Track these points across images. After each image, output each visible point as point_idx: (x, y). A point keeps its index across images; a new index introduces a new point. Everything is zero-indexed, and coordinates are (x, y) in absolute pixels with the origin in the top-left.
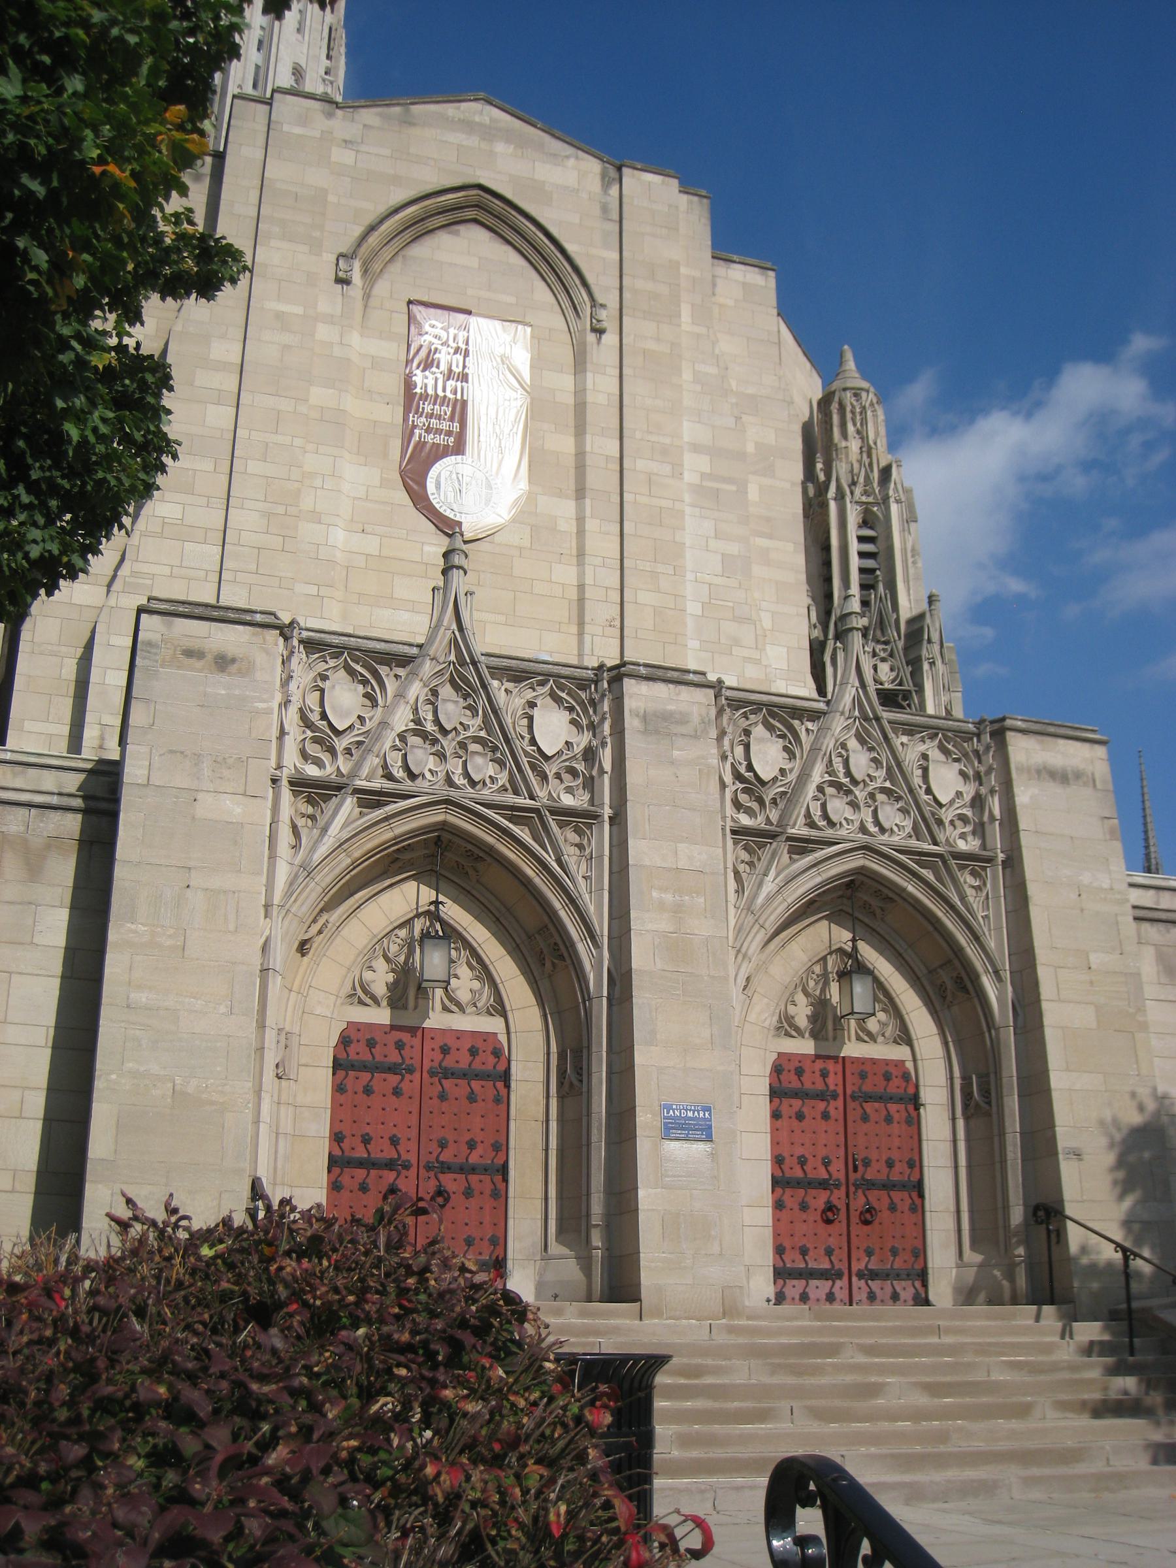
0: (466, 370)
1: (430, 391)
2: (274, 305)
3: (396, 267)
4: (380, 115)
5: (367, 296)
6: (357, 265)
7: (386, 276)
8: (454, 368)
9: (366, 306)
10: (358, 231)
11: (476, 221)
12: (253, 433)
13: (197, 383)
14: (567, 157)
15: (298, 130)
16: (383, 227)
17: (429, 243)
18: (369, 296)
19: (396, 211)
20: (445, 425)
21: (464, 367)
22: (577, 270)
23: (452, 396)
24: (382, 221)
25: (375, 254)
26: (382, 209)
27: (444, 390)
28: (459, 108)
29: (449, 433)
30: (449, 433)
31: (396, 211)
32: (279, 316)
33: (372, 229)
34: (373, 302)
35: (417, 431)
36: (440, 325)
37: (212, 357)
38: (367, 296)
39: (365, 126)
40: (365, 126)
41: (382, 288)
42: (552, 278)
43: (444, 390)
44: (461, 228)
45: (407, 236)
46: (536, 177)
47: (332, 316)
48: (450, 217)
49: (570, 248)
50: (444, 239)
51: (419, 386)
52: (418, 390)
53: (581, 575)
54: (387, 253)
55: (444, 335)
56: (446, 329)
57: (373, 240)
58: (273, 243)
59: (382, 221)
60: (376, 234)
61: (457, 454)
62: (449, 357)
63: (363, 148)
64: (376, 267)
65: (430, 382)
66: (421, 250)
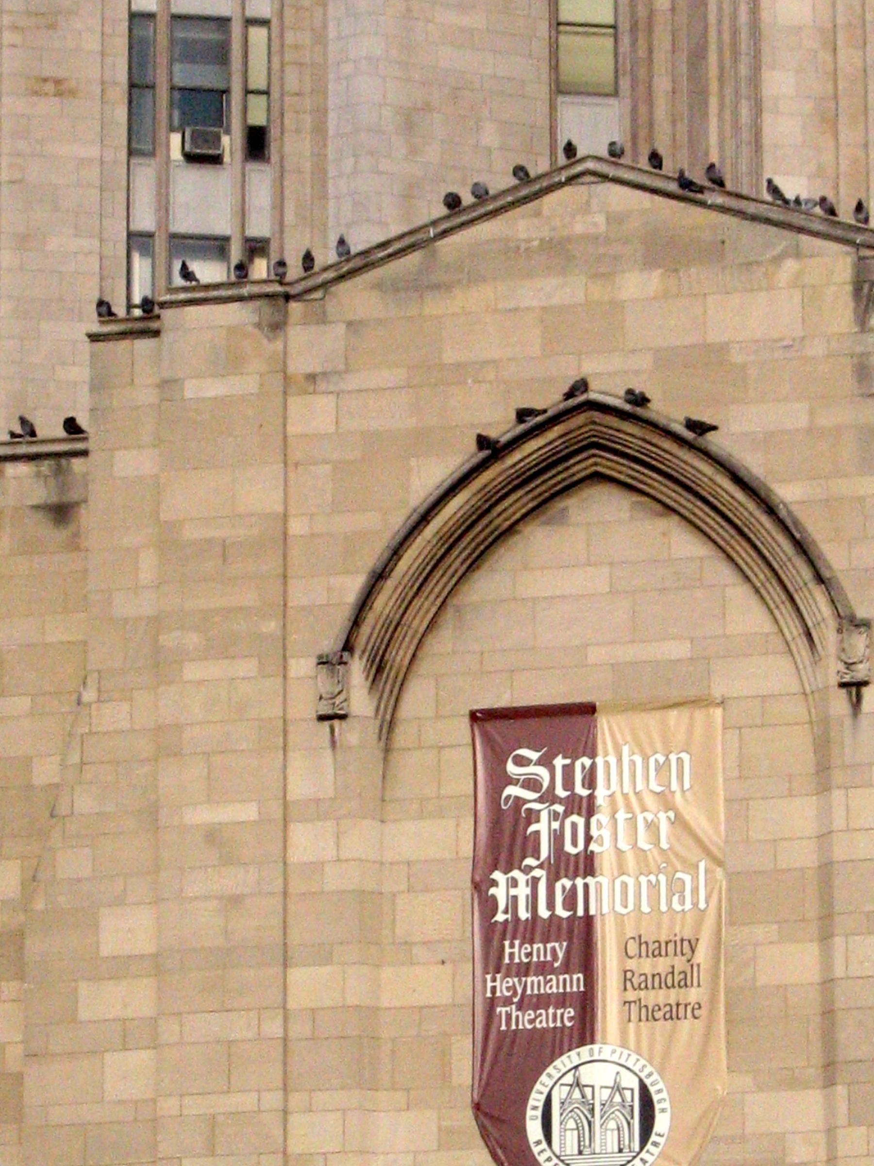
0: (593, 847)
1: (524, 914)
2: (203, 815)
3: (443, 642)
4: (379, 286)
5: (388, 727)
6: (357, 669)
7: (424, 666)
8: (569, 848)
9: (387, 750)
10: (353, 586)
11: (597, 477)
12: (187, 1100)
13: (84, 1014)
14: (777, 260)
15: (214, 388)
16: (403, 565)
17: (506, 560)
18: (392, 724)
19: (425, 518)
20: (554, 985)
21: (588, 839)
22: (801, 547)
23: (564, 914)
24: (396, 552)
25: (393, 628)
26: (398, 521)
27: (551, 905)
28: (538, 214)
29: (562, 1000)
30: (562, 1000)
31: (425, 518)
32: (212, 835)
33: (379, 577)
34: (403, 736)
35: (501, 1010)
36: (534, 755)
37: (106, 950)
38: (388, 727)
39: (350, 324)
40: (350, 324)
41: (418, 698)
42: (761, 574)
43: (551, 905)
44: (571, 503)
45: (456, 561)
46: (709, 340)
47: (318, 801)
48: (542, 486)
49: (787, 493)
50: (538, 541)
51: (502, 906)
52: (500, 917)
53: (836, 87)
54: (426, 605)
55: (543, 772)
56: (546, 762)
57: (384, 602)
58: (193, 672)
59: (396, 552)
60: (389, 585)
61: (582, 1043)
62: (556, 825)
63: (353, 382)
64: (399, 656)
65: (522, 891)
66: (489, 585)
